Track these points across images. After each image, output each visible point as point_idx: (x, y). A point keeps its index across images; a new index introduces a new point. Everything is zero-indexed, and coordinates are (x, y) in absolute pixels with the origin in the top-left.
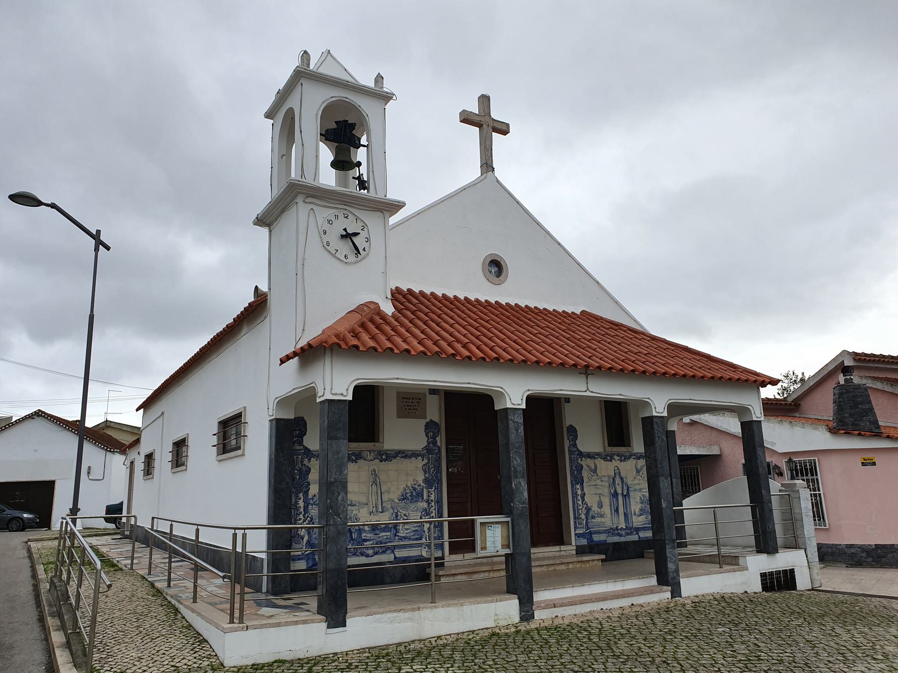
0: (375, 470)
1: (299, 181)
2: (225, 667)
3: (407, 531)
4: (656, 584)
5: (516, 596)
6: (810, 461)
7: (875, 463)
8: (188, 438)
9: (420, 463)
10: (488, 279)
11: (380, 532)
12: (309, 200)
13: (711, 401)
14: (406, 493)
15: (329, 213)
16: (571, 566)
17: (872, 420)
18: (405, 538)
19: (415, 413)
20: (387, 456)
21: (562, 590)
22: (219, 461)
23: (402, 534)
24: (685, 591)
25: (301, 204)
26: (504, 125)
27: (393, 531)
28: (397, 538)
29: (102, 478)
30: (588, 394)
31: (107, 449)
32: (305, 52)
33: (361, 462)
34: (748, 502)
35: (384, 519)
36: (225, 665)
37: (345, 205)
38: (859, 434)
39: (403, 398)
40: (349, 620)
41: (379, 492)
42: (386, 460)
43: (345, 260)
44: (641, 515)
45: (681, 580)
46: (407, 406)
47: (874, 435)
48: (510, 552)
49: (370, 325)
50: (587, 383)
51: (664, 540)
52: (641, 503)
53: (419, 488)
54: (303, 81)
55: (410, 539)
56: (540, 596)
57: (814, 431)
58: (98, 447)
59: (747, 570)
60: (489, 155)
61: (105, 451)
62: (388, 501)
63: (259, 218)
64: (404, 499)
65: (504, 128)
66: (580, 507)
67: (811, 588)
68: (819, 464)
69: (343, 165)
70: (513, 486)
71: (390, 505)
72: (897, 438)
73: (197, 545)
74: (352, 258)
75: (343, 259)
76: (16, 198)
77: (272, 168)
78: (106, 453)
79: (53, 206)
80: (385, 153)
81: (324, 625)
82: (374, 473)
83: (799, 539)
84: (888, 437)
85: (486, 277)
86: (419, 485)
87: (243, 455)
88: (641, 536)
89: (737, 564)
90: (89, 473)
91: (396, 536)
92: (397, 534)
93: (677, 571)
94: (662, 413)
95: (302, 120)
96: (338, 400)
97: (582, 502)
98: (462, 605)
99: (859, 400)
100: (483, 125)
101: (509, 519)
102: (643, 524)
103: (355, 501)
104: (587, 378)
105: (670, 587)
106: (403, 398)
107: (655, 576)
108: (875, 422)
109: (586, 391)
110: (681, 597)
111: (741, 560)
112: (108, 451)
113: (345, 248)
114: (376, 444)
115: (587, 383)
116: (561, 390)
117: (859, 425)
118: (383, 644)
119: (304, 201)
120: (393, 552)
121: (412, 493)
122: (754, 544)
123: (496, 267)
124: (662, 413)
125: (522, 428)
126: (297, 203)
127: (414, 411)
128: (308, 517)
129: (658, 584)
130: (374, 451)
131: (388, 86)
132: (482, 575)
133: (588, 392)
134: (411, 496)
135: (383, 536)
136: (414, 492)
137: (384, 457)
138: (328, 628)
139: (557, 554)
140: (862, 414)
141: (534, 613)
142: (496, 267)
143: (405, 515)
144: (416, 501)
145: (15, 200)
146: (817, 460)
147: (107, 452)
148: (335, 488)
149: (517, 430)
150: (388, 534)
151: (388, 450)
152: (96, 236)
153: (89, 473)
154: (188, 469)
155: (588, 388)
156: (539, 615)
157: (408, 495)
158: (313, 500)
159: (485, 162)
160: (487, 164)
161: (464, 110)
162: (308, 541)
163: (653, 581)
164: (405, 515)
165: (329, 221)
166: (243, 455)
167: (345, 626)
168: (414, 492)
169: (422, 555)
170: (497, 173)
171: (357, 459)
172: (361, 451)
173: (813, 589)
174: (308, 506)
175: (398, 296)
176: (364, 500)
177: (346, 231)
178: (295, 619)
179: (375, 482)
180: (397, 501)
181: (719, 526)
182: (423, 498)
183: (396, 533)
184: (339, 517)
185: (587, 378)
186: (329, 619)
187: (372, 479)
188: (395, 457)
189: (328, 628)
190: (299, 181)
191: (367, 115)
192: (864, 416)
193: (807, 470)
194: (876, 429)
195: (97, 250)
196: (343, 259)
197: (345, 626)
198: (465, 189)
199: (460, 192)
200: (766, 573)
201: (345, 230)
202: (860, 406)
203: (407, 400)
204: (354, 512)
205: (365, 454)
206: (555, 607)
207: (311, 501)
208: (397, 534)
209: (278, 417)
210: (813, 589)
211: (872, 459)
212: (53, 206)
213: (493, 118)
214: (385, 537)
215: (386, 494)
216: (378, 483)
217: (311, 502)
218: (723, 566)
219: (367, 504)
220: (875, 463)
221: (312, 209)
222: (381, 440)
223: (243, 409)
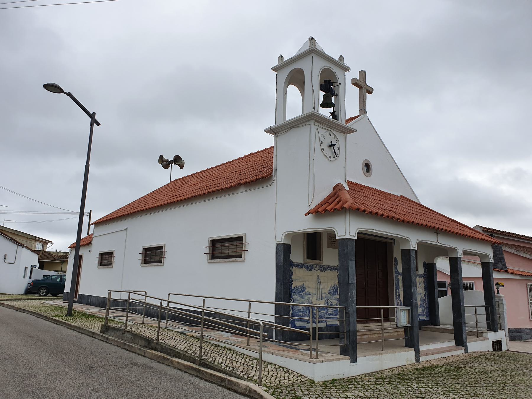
0: (318, 276)
1: (316, 113)
2: (315, 382)
3: (331, 311)
4: (455, 345)
5: (414, 349)
6: (470, 283)
7: (503, 286)
8: (165, 247)
9: (335, 274)
10: (364, 174)
11: (321, 310)
12: (316, 124)
13: (477, 251)
14: (331, 290)
15: (322, 132)
16: (399, 333)
17: (503, 263)
18: (331, 314)
19: (334, 245)
20: (324, 269)
21: (427, 346)
22: (209, 263)
23: (329, 312)
24: (470, 350)
25: (313, 126)
26: (371, 88)
27: (326, 310)
28: (327, 314)
29: (13, 262)
30: (437, 244)
31: (18, 244)
32: (312, 38)
33: (313, 270)
34: (484, 304)
35: (322, 303)
36: (315, 381)
37: (330, 128)
38: (498, 271)
39: (330, 237)
40: (359, 358)
41: (320, 288)
42: (323, 271)
43: (329, 159)
44: (420, 307)
45: (468, 343)
46: (331, 241)
47: (505, 272)
48: (410, 326)
49: (336, 196)
50: (437, 238)
51: (461, 322)
52: (421, 301)
53: (336, 287)
54: (313, 55)
55: (333, 315)
56: (422, 348)
57: (474, 267)
58: (13, 242)
59: (488, 339)
60: (365, 105)
61: (17, 245)
62: (324, 293)
63: (271, 129)
64: (330, 293)
65: (371, 90)
66: (398, 302)
67: (506, 350)
68: (475, 284)
69: (327, 105)
70: (412, 291)
71: (325, 296)
72: (531, 276)
73: (161, 311)
74: (332, 159)
75: (329, 158)
76: (47, 87)
77: (276, 100)
78: (17, 246)
79: (69, 94)
80: (345, 100)
81: (349, 361)
82: (318, 277)
83: (502, 325)
84: (512, 273)
85: (363, 172)
86: (336, 286)
87: (244, 261)
88: (420, 319)
89: (482, 336)
90: (5, 258)
91: (327, 313)
92: (328, 312)
93: (466, 339)
94: (281, 241)
95: (313, 77)
96: (352, 239)
97: (399, 299)
98: (396, 353)
99: (498, 253)
100: (362, 87)
101: (409, 308)
102: (421, 313)
103: (311, 293)
104: (437, 235)
105: (464, 347)
106: (330, 237)
107: (454, 341)
108: (505, 265)
109: (437, 242)
110: (468, 352)
111: (484, 335)
112: (19, 245)
113: (329, 152)
114: (320, 261)
115: (437, 238)
116: (429, 241)
117: (497, 266)
118: (369, 372)
119: (314, 124)
120: (326, 322)
121: (333, 290)
122: (453, 324)
123: (368, 167)
124: (281, 241)
125: (415, 260)
126: (310, 125)
127: (334, 245)
128: (292, 299)
129: (456, 345)
130: (318, 265)
131: (346, 62)
132: (366, 336)
133: (437, 243)
134: (333, 291)
135: (322, 313)
136: (334, 290)
137: (322, 269)
138: (351, 363)
139: (389, 326)
140: (499, 260)
141: (420, 358)
142: (368, 167)
143: (331, 302)
144: (335, 295)
145: (46, 88)
146: (474, 283)
147: (19, 246)
148: (352, 287)
149: (413, 261)
150: (324, 311)
151: (324, 265)
152: (92, 116)
153: (5, 258)
154: (164, 265)
155: (437, 241)
156: (422, 359)
157: (332, 291)
158: (294, 290)
159: (363, 108)
160: (364, 109)
161: (355, 78)
162: (292, 313)
163: (453, 343)
164: (331, 302)
165: (324, 136)
166: (244, 261)
167: (357, 362)
168: (334, 290)
169: (337, 324)
170: (369, 115)
171: (311, 269)
172: (313, 264)
173: (507, 351)
174: (292, 294)
175: (350, 183)
176: (314, 292)
177: (332, 143)
178: (332, 358)
179: (318, 282)
180: (327, 294)
181: (478, 316)
182: (338, 293)
183: (327, 311)
184: (353, 303)
185: (437, 235)
186: (351, 358)
187: (317, 281)
188: (327, 269)
189: (351, 363)
190: (316, 113)
191: (339, 79)
192: (499, 261)
193: (467, 287)
194: (505, 268)
195: (92, 125)
196: (329, 158)
197: (357, 362)
198: (356, 122)
199: (353, 124)
200: (493, 341)
201: (331, 142)
202: (498, 256)
203: (331, 238)
204: (311, 299)
205: (315, 266)
206: (427, 355)
207: (293, 290)
208: (328, 312)
209: (285, 243)
210: (507, 351)
211: (502, 284)
212: (69, 94)
213: (367, 85)
214: (323, 313)
215: (323, 289)
216: (320, 283)
217: (293, 291)
218: (480, 338)
219: (316, 295)
220: (503, 286)
221: (317, 129)
222: (322, 260)
223: (244, 235)
